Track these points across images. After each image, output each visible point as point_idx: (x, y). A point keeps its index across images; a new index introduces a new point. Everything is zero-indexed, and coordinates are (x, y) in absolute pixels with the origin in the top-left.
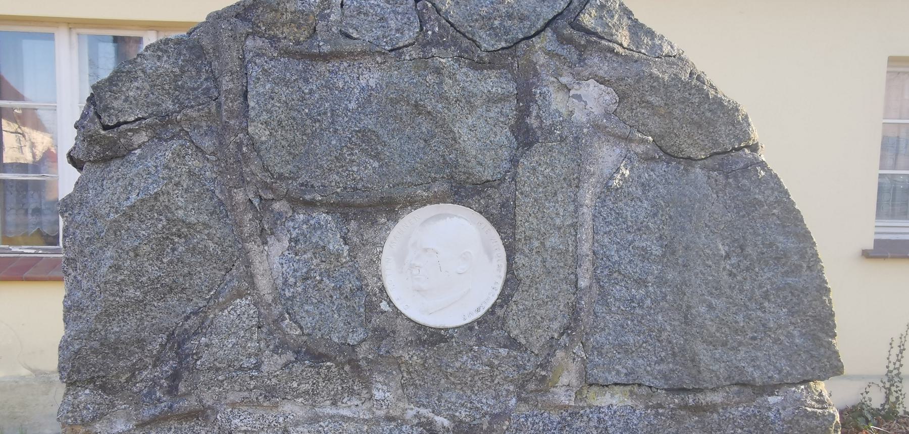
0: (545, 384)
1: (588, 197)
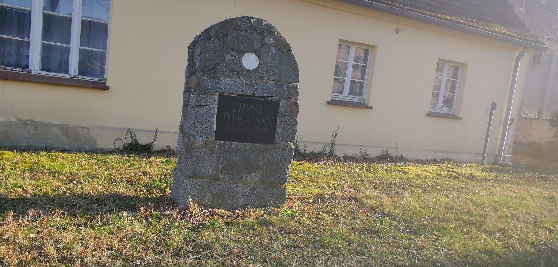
0: (263, 79)
1: (270, 54)
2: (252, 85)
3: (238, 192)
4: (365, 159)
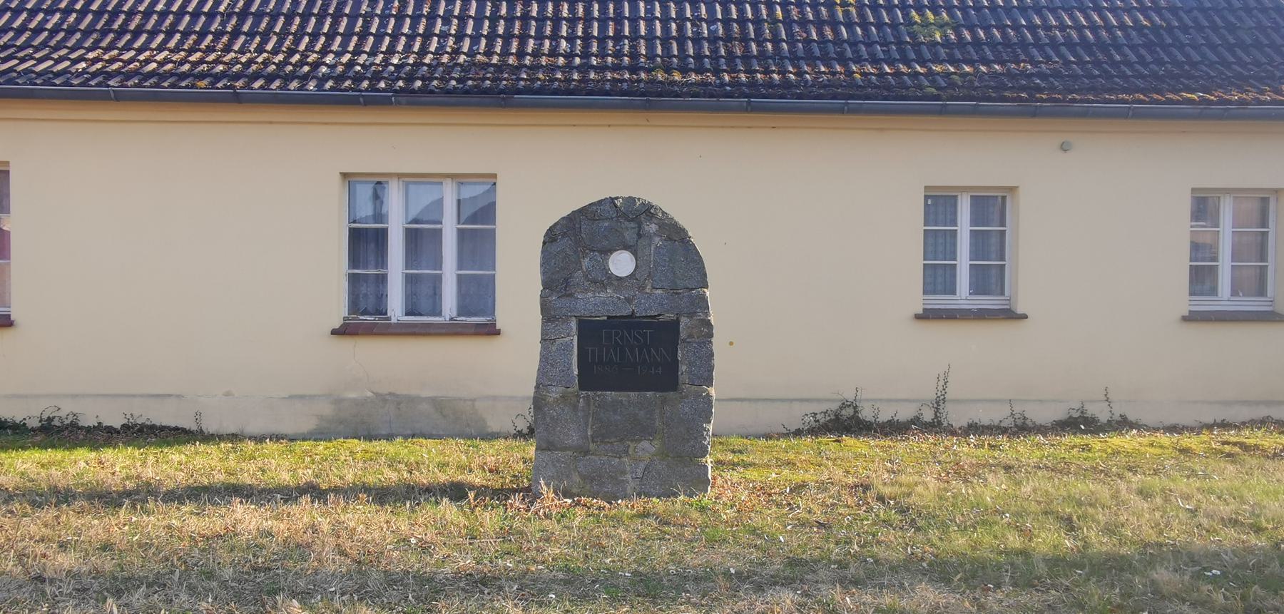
0: (644, 288)
2: (629, 300)
3: (624, 473)
4: (1022, 428)
